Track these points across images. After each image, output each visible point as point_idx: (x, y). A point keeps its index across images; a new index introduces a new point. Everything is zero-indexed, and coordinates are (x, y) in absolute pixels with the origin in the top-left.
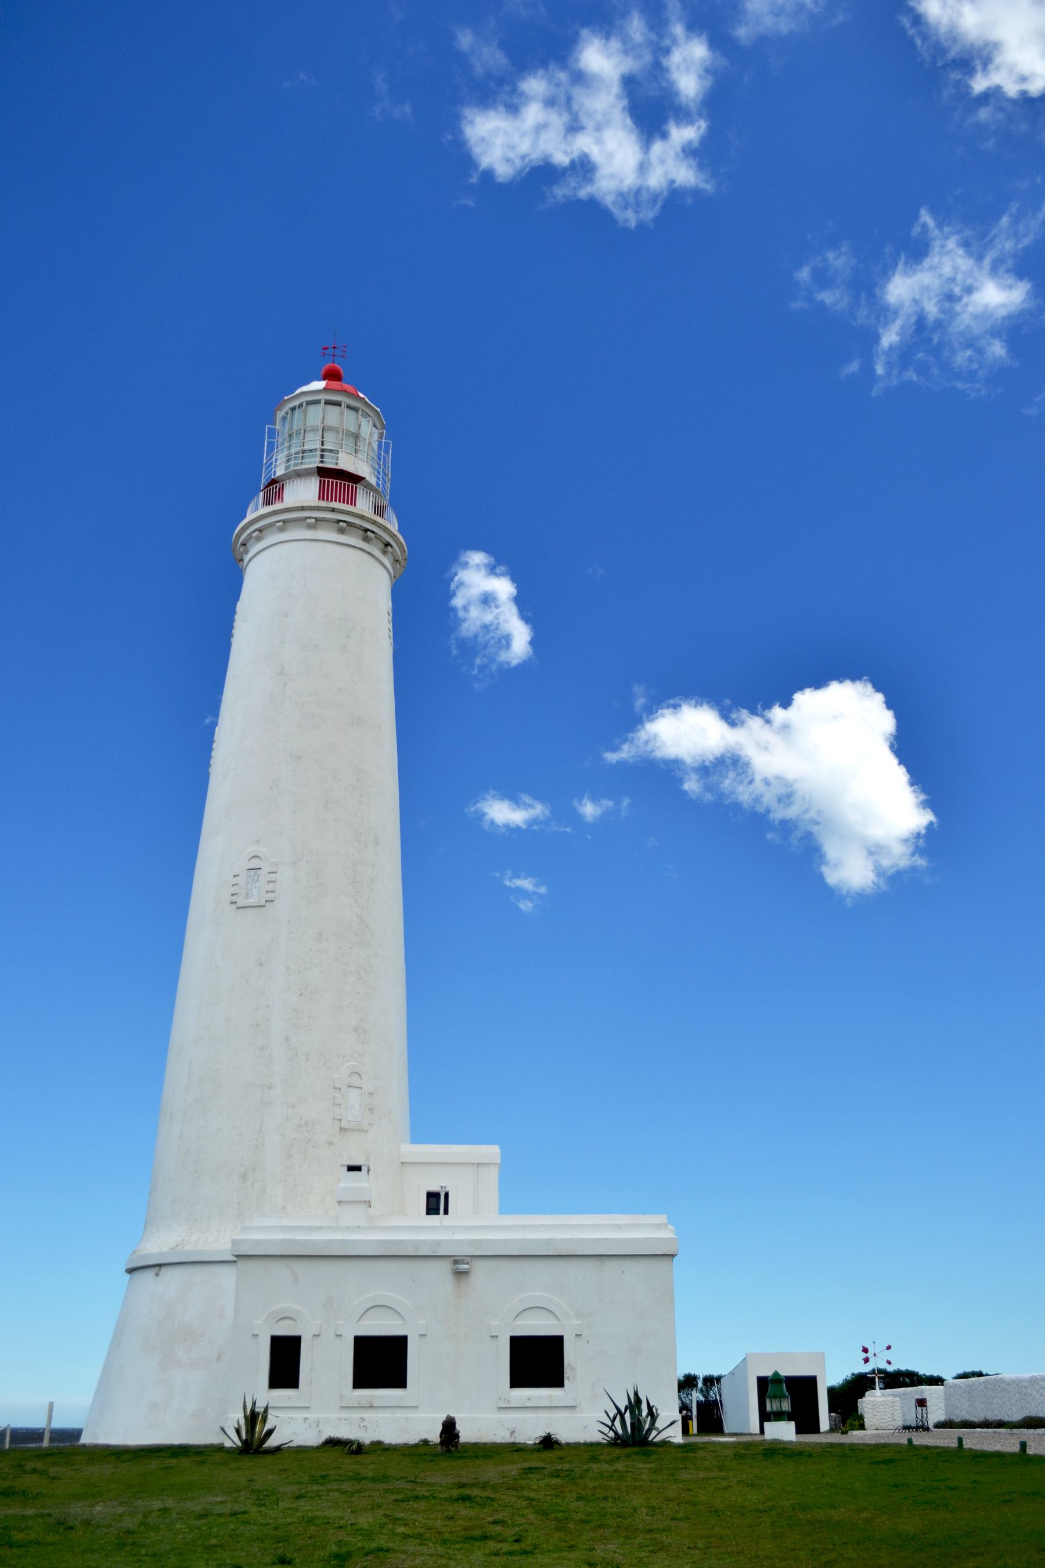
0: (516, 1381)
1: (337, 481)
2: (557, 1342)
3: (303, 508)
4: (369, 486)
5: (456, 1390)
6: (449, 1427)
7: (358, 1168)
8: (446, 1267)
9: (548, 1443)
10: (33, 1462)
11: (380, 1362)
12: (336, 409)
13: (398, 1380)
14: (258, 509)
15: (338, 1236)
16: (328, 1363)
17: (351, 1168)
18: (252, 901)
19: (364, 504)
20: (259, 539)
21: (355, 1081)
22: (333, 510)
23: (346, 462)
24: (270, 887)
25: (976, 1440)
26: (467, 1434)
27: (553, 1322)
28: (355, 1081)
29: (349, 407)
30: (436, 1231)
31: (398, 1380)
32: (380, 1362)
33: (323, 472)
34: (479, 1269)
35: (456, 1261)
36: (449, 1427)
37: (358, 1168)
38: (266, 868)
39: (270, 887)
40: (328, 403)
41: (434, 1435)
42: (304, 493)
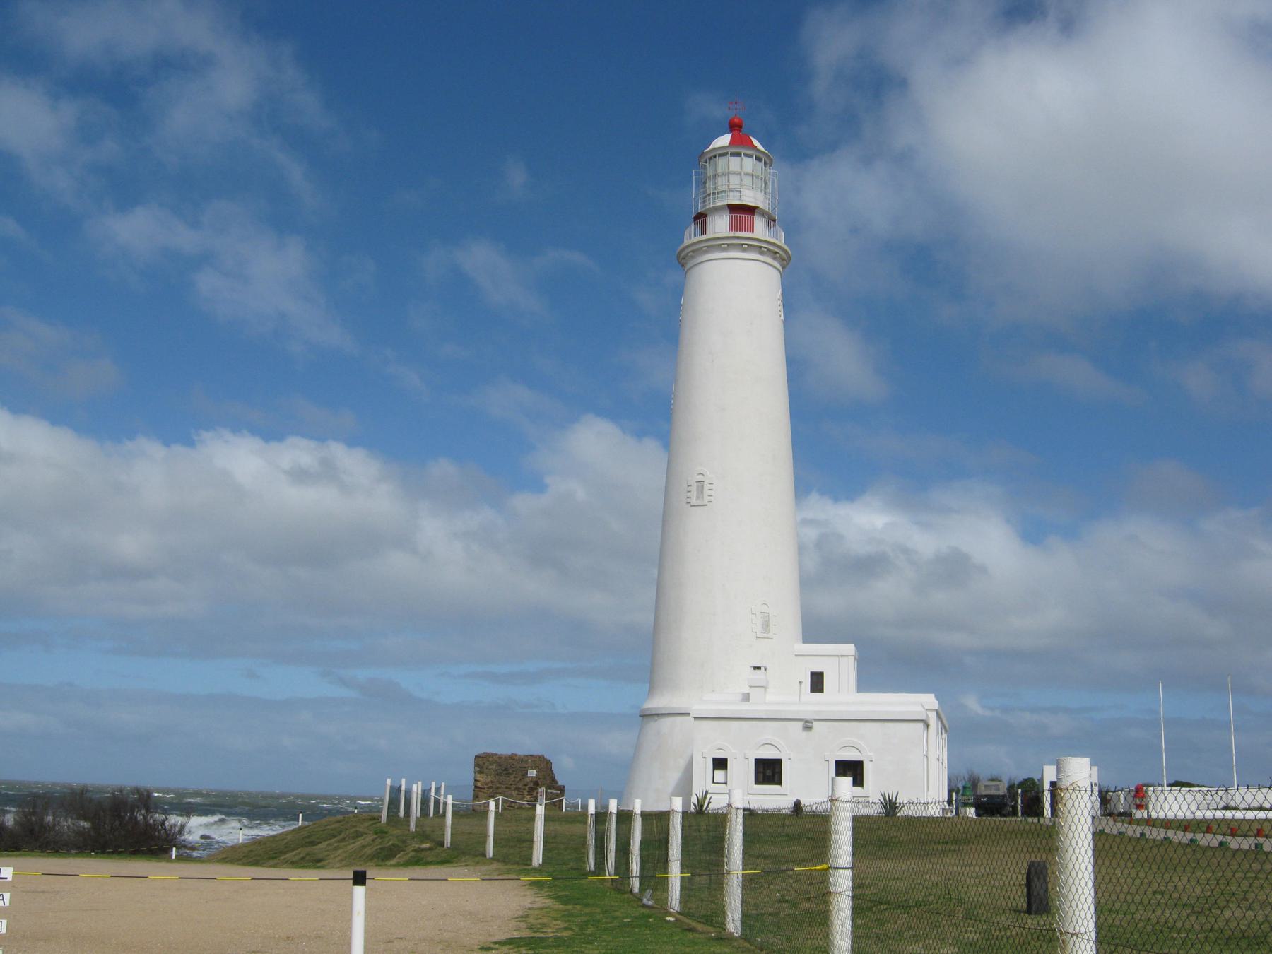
0: (758, 782)
1: (742, 212)
3: (719, 238)
4: (763, 213)
6: (797, 805)
7: (759, 668)
8: (800, 724)
10: (853, 951)
11: (768, 771)
12: (738, 159)
14: (691, 236)
17: (755, 668)
19: (760, 228)
22: (738, 238)
23: (749, 198)
25: (1205, 839)
29: (746, 155)
30: (812, 704)
32: (768, 771)
33: (733, 208)
34: (815, 724)
35: (806, 721)
36: (797, 805)
37: (759, 668)
40: (733, 154)
42: (720, 225)
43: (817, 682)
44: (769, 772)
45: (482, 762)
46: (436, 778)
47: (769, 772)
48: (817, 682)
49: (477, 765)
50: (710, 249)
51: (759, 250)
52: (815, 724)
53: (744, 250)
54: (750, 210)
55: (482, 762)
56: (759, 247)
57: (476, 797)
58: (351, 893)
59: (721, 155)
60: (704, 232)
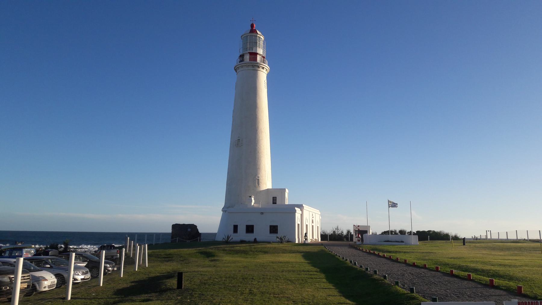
11: (250, 229)
16: (242, 229)
55: (175, 227)
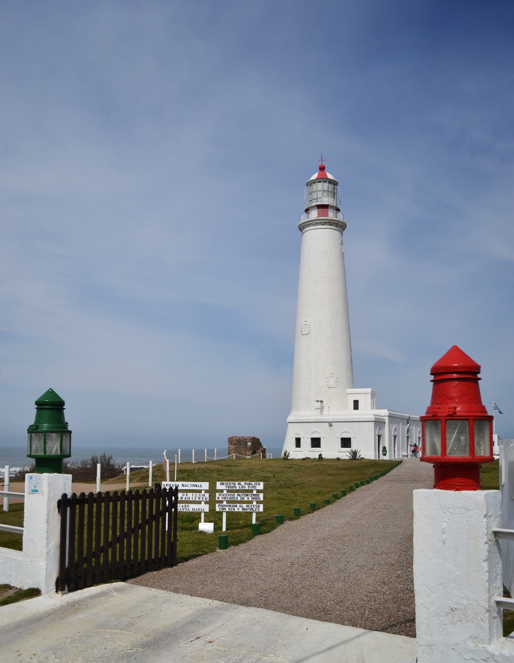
0: (342, 447)
2: (320, 438)
3: (311, 221)
5: (332, 450)
9: (338, 459)
11: (316, 442)
13: (313, 446)
15: (307, 418)
16: (306, 443)
18: (305, 333)
20: (307, 227)
21: (332, 375)
24: (309, 329)
26: (323, 456)
27: (349, 435)
28: (332, 375)
31: (313, 446)
33: (319, 207)
35: (329, 423)
38: (308, 324)
39: (309, 329)
40: (318, 182)
41: (317, 457)
43: (356, 405)
44: (316, 443)
45: (231, 441)
46: (218, 448)
47: (316, 443)
48: (356, 405)
49: (229, 441)
50: (309, 225)
51: (316, 224)
52: (333, 424)
53: (323, 225)
54: (325, 207)
55: (231, 441)
56: (331, 223)
57: (229, 454)
58: (3, 499)
59: (314, 183)
60: (309, 218)
